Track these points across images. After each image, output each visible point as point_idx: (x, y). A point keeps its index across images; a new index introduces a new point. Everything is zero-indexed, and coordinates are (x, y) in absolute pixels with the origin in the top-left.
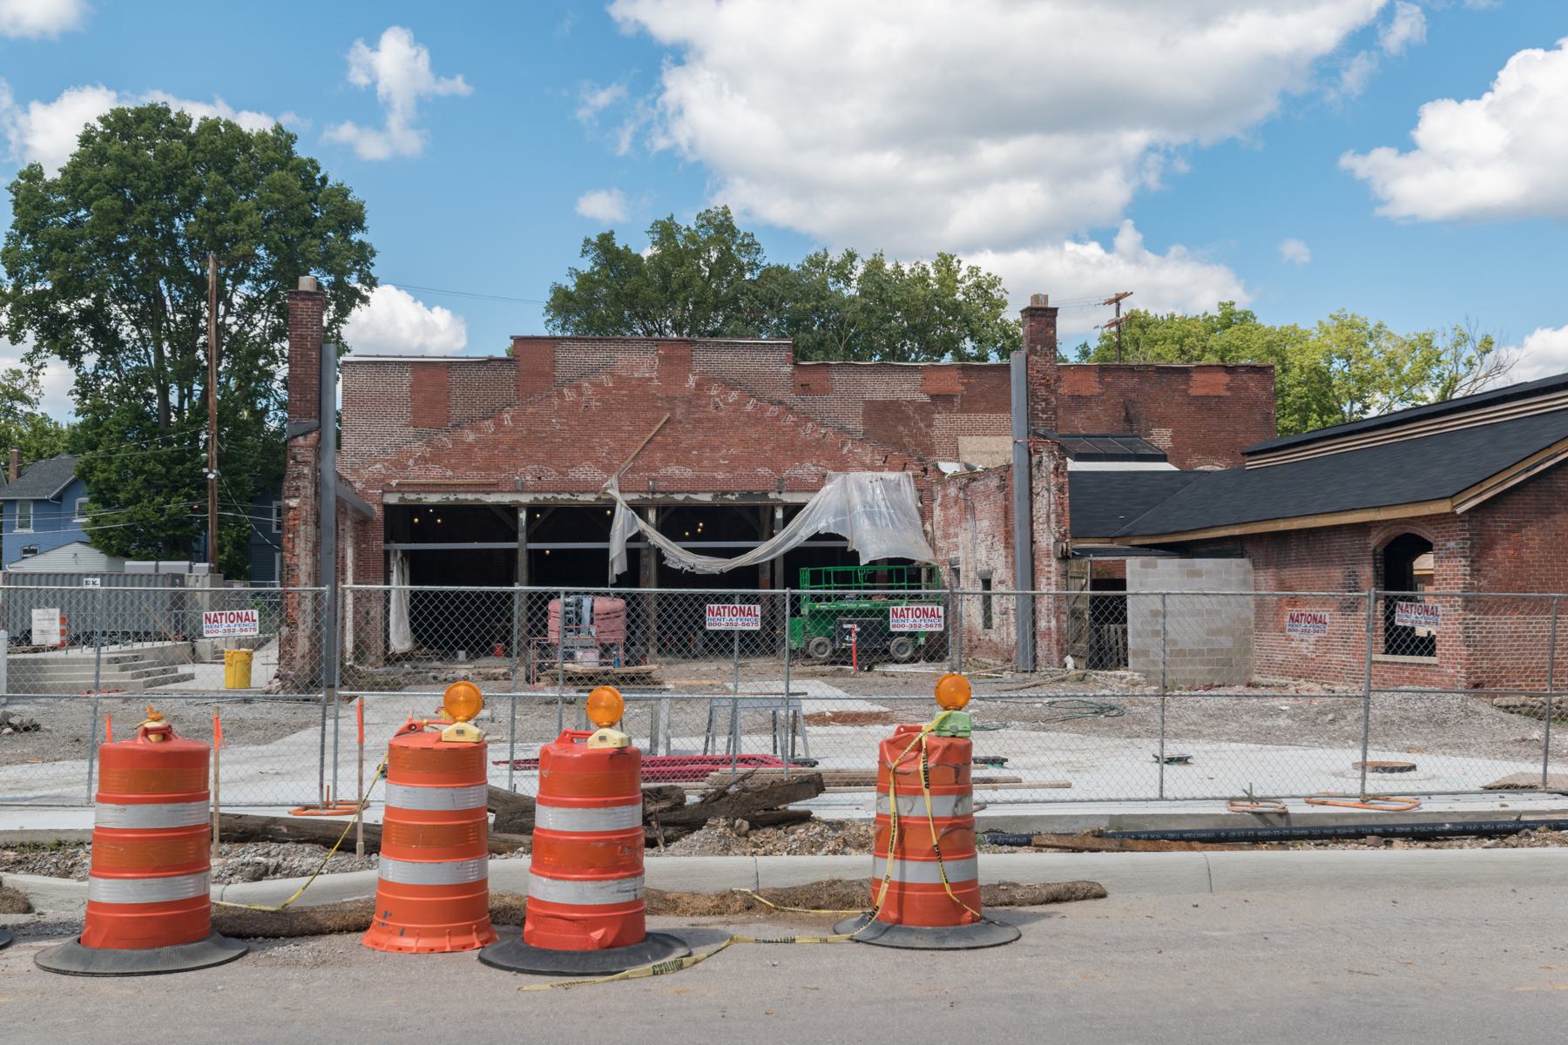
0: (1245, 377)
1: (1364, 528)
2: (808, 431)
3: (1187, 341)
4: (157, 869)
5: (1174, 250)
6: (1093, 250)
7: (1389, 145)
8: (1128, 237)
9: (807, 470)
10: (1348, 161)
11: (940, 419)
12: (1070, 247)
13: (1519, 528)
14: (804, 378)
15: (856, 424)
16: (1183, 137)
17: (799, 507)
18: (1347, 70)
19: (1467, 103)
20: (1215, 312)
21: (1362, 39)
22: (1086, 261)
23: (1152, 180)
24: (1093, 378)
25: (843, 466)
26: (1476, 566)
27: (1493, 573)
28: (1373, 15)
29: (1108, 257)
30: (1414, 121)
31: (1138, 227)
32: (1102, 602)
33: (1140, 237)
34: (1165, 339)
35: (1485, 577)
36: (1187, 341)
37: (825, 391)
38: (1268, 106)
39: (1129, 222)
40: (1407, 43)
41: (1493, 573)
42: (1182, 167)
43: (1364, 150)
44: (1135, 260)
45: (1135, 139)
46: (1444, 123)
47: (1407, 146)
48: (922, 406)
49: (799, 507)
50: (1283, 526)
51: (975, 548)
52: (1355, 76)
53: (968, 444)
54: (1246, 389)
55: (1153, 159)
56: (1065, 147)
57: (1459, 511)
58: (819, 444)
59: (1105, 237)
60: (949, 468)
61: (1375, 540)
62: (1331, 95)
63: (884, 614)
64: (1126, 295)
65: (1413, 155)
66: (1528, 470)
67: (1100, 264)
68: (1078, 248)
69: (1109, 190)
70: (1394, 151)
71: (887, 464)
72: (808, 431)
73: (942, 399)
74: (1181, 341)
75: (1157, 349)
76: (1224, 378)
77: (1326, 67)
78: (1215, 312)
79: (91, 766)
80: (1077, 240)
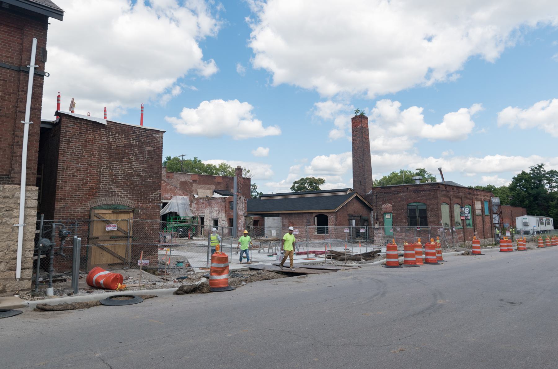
1: (312, 213)
2: (169, 187)
9: (168, 195)
11: (194, 185)
14: (168, 175)
15: (178, 186)
17: (167, 203)
19: (192, 109)
21: (168, 91)
24: (221, 179)
25: (175, 195)
30: (181, 110)
37: (173, 178)
46: (188, 113)
47: (179, 117)
48: (191, 183)
49: (167, 203)
50: (293, 212)
51: (210, 214)
53: (199, 191)
58: (171, 189)
60: (196, 196)
63: (359, 228)
71: (184, 195)
72: (169, 187)
73: (195, 181)
77: (160, 96)
79: (208, 256)
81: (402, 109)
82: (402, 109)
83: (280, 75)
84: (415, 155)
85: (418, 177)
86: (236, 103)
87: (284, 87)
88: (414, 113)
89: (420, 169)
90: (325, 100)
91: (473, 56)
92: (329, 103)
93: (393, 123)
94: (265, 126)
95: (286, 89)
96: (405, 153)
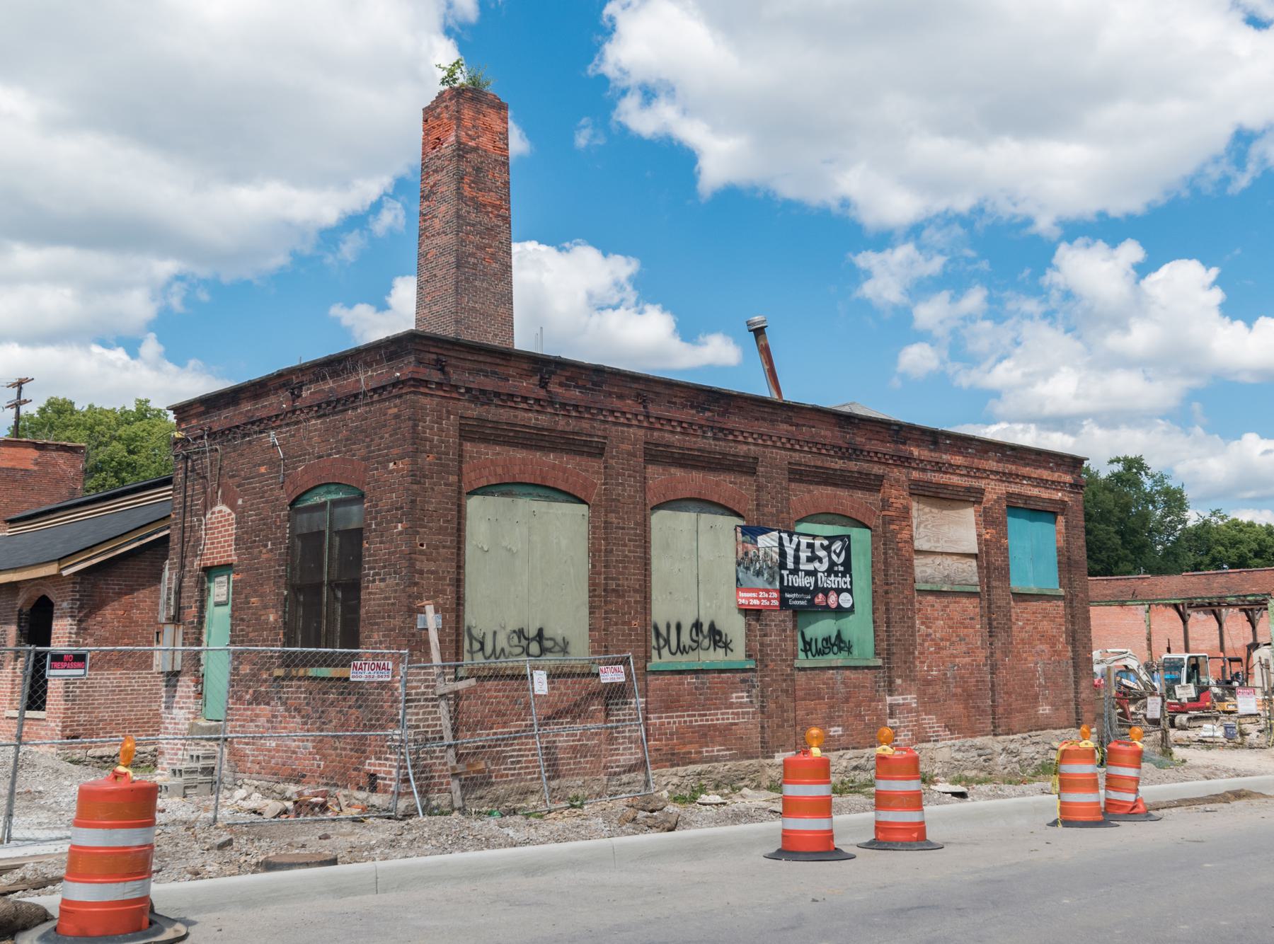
0: (54, 454)
3: (97, 428)
4: (124, 876)
5: (192, 363)
6: (119, 355)
7: (370, 303)
8: (151, 347)
10: (336, 311)
12: (96, 349)
13: (131, 590)
16: (204, 272)
18: (344, 243)
20: (132, 407)
21: (355, 222)
22: (112, 364)
23: (176, 302)
26: (84, 625)
27: (100, 632)
28: (367, 208)
29: (133, 362)
31: (160, 340)
32: (289, 656)
33: (161, 349)
34: (79, 425)
35: (91, 635)
36: (97, 428)
38: (280, 260)
39: (153, 335)
40: (391, 231)
41: (100, 632)
42: (204, 296)
43: (350, 305)
44: (157, 368)
45: (166, 267)
52: (351, 246)
54: (55, 465)
55: (176, 287)
56: (102, 263)
57: (65, 573)
59: (133, 347)
61: (21, 600)
62: (329, 259)
64: (27, 380)
65: (387, 313)
66: (140, 539)
67: (126, 368)
68: (105, 351)
69: (137, 306)
70: (373, 309)
74: (91, 429)
75: (68, 433)
76: (33, 454)
77: (329, 237)
78: (132, 407)
80: (105, 344)
81: (1142, 270)
82: (1142, 270)
83: (721, 157)
84: (1198, 430)
85: (677, 400)
86: (588, 256)
87: (734, 199)
88: (1186, 283)
89: (1126, 459)
90: (883, 240)
91: (693, 152)
92: (904, 252)
93: (1119, 321)
94: (688, 332)
95: (746, 207)
96: (1162, 425)
